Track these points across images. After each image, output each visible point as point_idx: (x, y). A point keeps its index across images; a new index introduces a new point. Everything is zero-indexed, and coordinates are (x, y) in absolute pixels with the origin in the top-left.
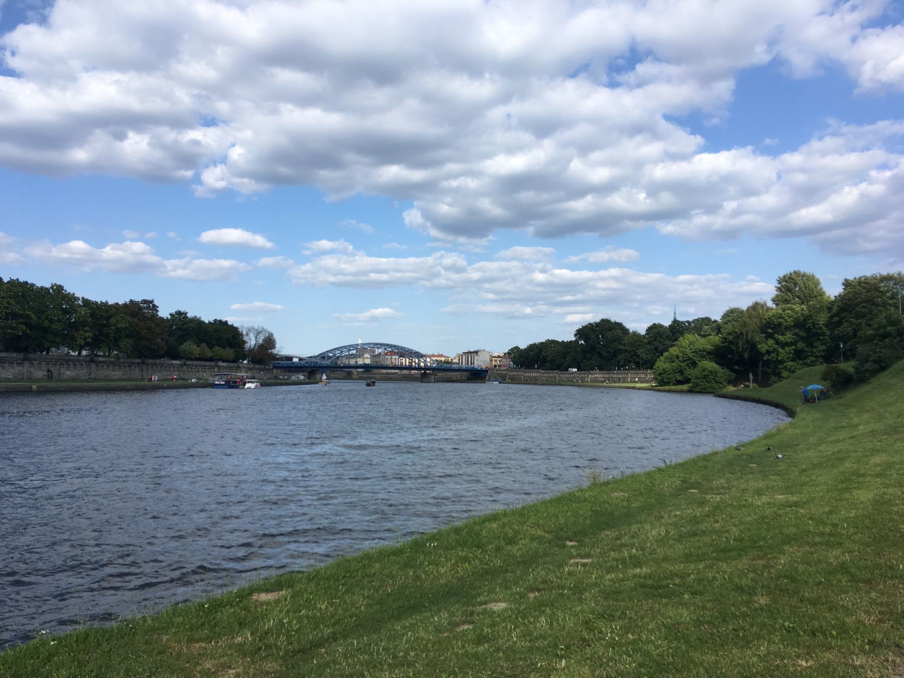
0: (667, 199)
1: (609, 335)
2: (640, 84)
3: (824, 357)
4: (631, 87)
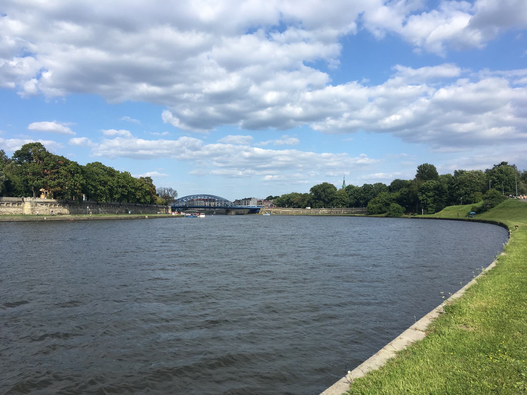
0: (313, 110)
1: (329, 190)
2: (289, 42)
3: (446, 202)
4: (281, 44)
